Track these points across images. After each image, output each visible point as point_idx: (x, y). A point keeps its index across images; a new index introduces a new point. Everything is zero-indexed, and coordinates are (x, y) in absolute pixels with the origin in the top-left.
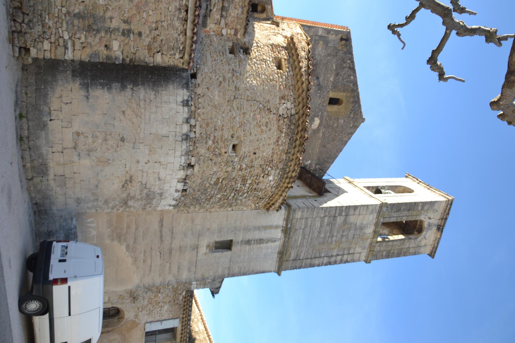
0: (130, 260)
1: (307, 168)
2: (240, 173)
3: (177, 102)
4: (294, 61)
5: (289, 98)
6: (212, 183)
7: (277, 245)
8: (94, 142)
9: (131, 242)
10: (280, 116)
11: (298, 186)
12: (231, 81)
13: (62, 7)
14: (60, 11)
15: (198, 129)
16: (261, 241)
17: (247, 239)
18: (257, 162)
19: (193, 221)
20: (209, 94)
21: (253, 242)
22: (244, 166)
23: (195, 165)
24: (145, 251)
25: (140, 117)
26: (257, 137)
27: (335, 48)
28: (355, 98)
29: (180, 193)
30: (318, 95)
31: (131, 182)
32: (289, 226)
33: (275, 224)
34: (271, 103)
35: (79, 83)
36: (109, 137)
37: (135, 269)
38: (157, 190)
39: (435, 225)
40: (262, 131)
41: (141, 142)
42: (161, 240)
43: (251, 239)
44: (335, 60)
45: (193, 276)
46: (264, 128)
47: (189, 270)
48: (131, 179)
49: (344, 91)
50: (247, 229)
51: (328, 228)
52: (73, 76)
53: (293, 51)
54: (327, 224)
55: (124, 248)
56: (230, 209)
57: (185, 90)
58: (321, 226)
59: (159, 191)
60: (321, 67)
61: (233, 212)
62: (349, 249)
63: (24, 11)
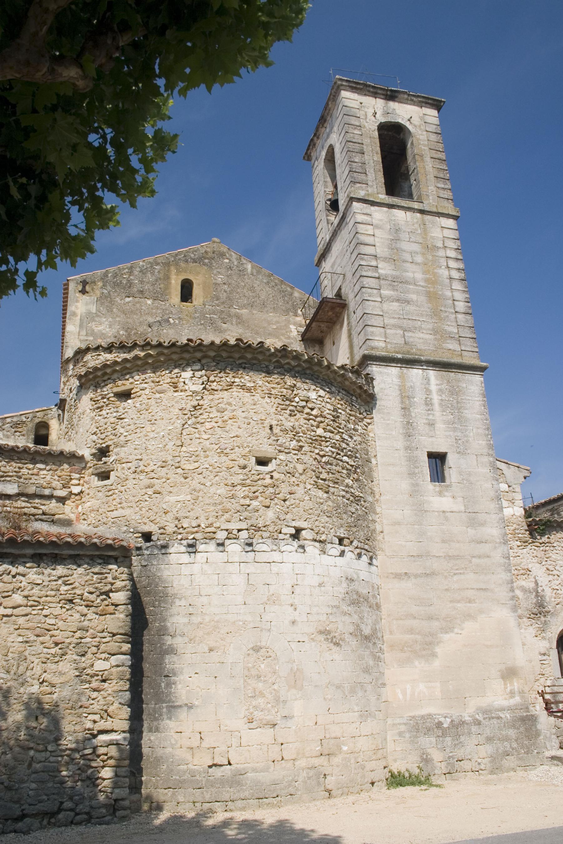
0: (469, 625)
1: (302, 330)
2: (306, 448)
4: (115, 371)
5: (174, 376)
7: (432, 374)
8: (262, 694)
10: (204, 388)
11: (334, 344)
12: (152, 475)
13: (46, 750)
14: (53, 754)
15: (234, 526)
18: (284, 422)
19: (397, 523)
20: (174, 511)
21: (431, 417)
22: (294, 443)
23: (294, 527)
24: (451, 601)
25: (218, 622)
28: (180, 259)
29: (347, 549)
31: (329, 632)
34: (184, 406)
35: (168, 721)
36: (254, 672)
38: (342, 589)
41: (259, 619)
42: (432, 574)
45: (494, 516)
47: (483, 524)
48: (325, 632)
52: (157, 730)
53: (109, 371)
54: (394, 290)
55: (446, 637)
56: (374, 461)
58: (398, 300)
59: (344, 585)
63: (56, 809)
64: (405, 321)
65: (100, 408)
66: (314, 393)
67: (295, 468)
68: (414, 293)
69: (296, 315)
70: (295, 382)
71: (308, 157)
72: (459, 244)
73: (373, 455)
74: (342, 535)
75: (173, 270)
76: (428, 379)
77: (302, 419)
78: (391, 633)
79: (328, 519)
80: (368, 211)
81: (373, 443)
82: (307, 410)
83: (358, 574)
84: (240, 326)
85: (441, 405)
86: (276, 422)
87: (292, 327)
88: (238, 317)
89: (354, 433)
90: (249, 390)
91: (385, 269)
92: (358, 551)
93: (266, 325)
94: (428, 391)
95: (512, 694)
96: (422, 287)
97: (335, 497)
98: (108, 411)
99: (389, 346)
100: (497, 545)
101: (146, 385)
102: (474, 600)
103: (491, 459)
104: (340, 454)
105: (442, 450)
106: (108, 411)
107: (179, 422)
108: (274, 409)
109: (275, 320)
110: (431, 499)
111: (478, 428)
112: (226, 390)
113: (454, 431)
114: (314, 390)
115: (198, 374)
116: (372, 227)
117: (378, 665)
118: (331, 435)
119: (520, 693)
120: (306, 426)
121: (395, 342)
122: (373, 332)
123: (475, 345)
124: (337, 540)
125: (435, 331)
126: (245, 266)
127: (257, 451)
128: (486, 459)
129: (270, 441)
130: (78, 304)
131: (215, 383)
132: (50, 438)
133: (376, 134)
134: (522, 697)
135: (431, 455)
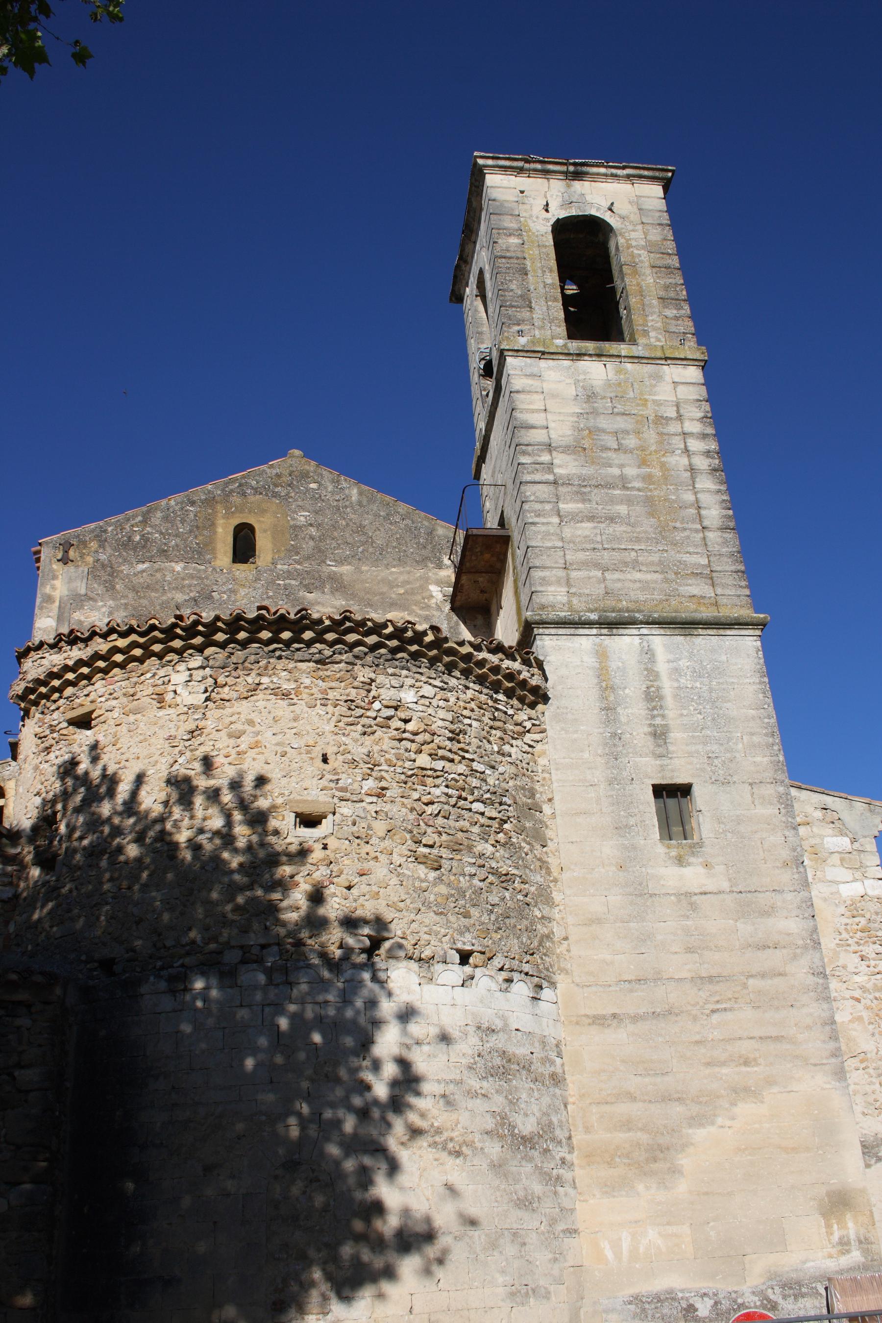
0: (745, 1109)
2: (394, 791)
3: (174, 1011)
5: (160, 682)
6: (432, 875)
7: (660, 642)
9: (678, 1109)
10: (207, 699)
16: (653, 698)
17: (650, 742)
19: (596, 920)
21: (658, 721)
22: (370, 784)
24: (708, 1064)
26: (272, 758)
27: (92, 574)
28: (232, 491)
30: (225, 596)
32: (594, 617)
33: (591, 661)
34: (173, 732)
37: (775, 1089)
39: (569, 186)
40: (256, 745)
43: (647, 729)
44: (125, 568)
45: (789, 896)
46: (244, 742)
47: (768, 912)
49: (213, 525)
50: (614, 743)
51: (597, 495)
54: (584, 501)
55: (699, 1134)
56: (547, 809)
57: (144, 989)
58: (592, 518)
60: (144, 602)
61: (556, 799)
62: (661, 420)
64: (605, 553)
65: (48, 750)
66: (412, 692)
67: (370, 828)
68: (621, 502)
69: (440, 566)
70: (373, 676)
71: (458, 298)
72: (708, 408)
73: (545, 798)
74: (468, 947)
75: (221, 510)
76: (649, 653)
77: (386, 740)
78: (587, 1130)
79: (437, 918)
80: (535, 370)
81: (546, 775)
82: (396, 723)
83: (504, 1018)
84: (337, 594)
85: (675, 696)
86: (335, 749)
87: (434, 589)
88: (333, 578)
89: (499, 758)
90: (286, 695)
91: (566, 466)
92: (505, 975)
93: (385, 589)
94: (651, 674)
95: (844, 1245)
96: (639, 490)
97: (452, 878)
98: (58, 753)
99: (575, 601)
100: (798, 951)
101: (114, 703)
102: (755, 1059)
103: (781, 789)
104: (466, 799)
105: (681, 779)
106: (58, 753)
107: (164, 761)
108: (333, 724)
109: (401, 578)
110: (662, 871)
111: (752, 734)
112: (246, 698)
113: (705, 744)
114: (412, 686)
115: (198, 675)
116: (541, 397)
117: (555, 1193)
118: (448, 765)
119: (860, 1242)
120: (393, 751)
121: (587, 592)
122: (543, 579)
123: (744, 583)
124: (457, 956)
125: (662, 567)
126: (347, 491)
127: (298, 801)
128: (769, 791)
129: (324, 782)
130: (55, 582)
131: (227, 689)
132: (6, 811)
133: (550, 238)
134: (866, 1252)
135: (660, 791)
